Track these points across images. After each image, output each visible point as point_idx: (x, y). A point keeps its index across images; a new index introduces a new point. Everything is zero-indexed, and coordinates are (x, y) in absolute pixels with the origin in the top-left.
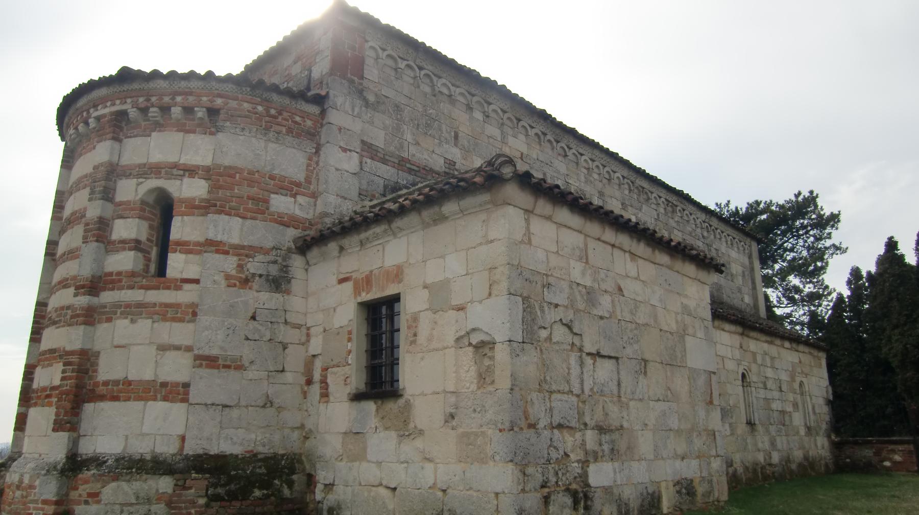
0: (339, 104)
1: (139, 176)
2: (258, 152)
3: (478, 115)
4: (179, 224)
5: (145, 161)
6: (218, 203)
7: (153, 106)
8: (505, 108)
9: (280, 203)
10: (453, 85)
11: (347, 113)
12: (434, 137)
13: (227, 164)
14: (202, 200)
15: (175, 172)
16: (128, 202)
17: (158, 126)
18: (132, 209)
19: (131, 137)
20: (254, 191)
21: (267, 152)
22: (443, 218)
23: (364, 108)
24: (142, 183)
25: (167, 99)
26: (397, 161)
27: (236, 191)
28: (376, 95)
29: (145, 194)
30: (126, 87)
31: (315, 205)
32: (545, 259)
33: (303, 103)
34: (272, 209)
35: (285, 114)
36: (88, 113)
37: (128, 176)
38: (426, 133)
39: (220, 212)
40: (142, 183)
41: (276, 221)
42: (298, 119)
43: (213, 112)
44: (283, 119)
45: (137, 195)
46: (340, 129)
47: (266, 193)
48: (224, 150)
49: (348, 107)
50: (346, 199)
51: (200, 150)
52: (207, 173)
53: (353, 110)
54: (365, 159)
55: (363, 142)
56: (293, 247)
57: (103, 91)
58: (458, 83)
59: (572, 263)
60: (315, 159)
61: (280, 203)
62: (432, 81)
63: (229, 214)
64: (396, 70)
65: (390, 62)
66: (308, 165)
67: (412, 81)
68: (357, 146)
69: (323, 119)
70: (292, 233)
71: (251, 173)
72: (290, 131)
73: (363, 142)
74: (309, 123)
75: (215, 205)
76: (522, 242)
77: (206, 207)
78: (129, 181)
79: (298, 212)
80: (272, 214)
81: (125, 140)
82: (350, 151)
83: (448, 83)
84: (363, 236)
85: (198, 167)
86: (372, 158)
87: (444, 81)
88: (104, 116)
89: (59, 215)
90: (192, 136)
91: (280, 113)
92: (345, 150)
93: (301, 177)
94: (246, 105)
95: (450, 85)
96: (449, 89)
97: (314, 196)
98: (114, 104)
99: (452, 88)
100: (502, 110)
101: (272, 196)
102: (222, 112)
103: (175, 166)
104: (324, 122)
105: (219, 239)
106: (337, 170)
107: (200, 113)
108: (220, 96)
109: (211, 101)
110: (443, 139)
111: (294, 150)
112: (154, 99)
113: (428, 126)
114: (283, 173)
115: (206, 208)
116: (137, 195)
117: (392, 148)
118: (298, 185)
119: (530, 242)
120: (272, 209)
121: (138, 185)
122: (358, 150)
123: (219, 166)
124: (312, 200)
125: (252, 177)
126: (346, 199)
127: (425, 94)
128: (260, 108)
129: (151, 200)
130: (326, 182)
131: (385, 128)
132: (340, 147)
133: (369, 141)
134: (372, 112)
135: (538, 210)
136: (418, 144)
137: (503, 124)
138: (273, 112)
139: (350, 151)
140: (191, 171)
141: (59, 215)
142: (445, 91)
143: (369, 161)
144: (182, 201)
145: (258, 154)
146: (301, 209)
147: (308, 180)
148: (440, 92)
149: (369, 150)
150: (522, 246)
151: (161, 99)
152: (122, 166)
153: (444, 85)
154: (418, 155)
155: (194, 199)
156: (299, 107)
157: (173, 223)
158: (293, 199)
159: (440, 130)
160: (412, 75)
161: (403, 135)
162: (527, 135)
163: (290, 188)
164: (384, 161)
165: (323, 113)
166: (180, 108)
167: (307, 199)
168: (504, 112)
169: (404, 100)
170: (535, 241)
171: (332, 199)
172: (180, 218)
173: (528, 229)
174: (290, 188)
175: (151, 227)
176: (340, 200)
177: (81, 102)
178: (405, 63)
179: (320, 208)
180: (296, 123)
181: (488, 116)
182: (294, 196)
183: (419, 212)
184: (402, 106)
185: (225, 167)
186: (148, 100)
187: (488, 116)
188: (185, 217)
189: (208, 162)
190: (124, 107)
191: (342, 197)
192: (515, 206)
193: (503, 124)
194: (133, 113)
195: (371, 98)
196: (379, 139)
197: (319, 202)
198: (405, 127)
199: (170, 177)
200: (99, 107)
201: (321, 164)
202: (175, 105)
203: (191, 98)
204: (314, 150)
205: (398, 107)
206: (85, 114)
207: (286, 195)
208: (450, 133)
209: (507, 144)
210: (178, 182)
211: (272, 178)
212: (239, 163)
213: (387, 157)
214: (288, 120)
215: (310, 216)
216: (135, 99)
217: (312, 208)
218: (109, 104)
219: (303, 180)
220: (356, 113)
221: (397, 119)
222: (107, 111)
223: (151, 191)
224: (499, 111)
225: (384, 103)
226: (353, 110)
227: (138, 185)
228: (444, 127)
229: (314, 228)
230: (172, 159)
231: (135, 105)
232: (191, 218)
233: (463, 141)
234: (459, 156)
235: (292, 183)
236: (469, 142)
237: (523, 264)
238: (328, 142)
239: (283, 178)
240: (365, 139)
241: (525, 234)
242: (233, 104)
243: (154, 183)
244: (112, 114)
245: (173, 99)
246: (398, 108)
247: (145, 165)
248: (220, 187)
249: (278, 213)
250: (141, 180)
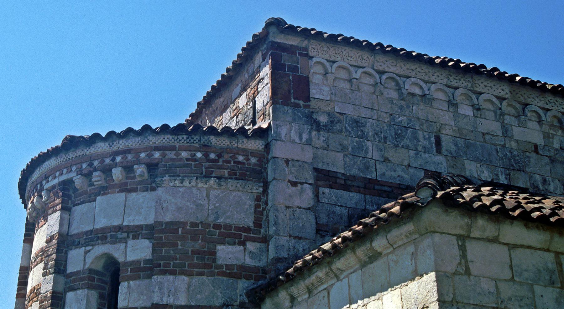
0: (283, 135)
1: (86, 244)
2: (200, 202)
3: (466, 110)
4: (125, 291)
5: (90, 228)
6: (162, 263)
7: (95, 170)
8: (502, 94)
9: (227, 254)
10: (426, 82)
11: (293, 142)
12: (408, 148)
13: (168, 220)
14: (146, 261)
15: (120, 235)
16: (78, 273)
17: (103, 190)
18: (82, 279)
19: (78, 204)
20: (198, 245)
21: (209, 200)
22: (375, 256)
23: (314, 133)
24: (89, 251)
25: (108, 161)
26: (362, 184)
27: (180, 247)
28: (329, 114)
29: (92, 263)
30: (71, 155)
31: (268, 251)
32: (493, 289)
33: (245, 140)
34: (220, 262)
35: (226, 156)
36: (41, 185)
37: (78, 245)
38: (397, 146)
39: (163, 273)
40: (89, 251)
41: (223, 274)
42: (241, 158)
43: (152, 167)
44: (224, 162)
45: (85, 264)
46: (287, 161)
47: (211, 246)
48: (164, 205)
49: (294, 135)
50: (300, 238)
51: (141, 208)
52: (148, 231)
53: (301, 138)
54: (321, 190)
55: (316, 170)
56: (247, 301)
57: (52, 163)
58: (432, 79)
59: (538, 289)
60: (264, 199)
61: (227, 254)
62: (397, 84)
63: (173, 273)
64: (350, 81)
65: (343, 74)
66: (257, 206)
67: (372, 90)
68: (309, 176)
69: (268, 154)
70: (243, 285)
71: (194, 225)
72: (233, 175)
73: (316, 170)
74: (253, 160)
75: (159, 265)
76: (456, 273)
77: (146, 270)
78: (77, 250)
79: (249, 262)
80: (221, 266)
81: (73, 209)
82: (302, 183)
83: (419, 81)
84: (308, 281)
85: (141, 227)
86: (330, 187)
87: (413, 80)
88: (54, 187)
89: (23, 292)
90: (134, 195)
91: (219, 156)
92: (294, 184)
93: (249, 222)
94: (184, 154)
95: (421, 83)
96: (421, 87)
97: (265, 240)
98: (61, 174)
99: (424, 86)
100: (498, 97)
101: (219, 247)
102: (160, 165)
103: (119, 228)
104: (269, 158)
105: (165, 302)
106: (287, 207)
107: (140, 170)
108: (157, 149)
109: (149, 156)
110: (420, 148)
111: (239, 193)
112: (96, 163)
113: (398, 136)
114: (228, 221)
115: (151, 269)
116: (85, 264)
117: (354, 172)
118: (247, 230)
119: (468, 272)
120: (220, 262)
121: (86, 252)
122: (311, 181)
123: (160, 223)
124: (263, 246)
125: (196, 230)
126: (300, 238)
127: (391, 101)
128: (199, 155)
129: (99, 266)
130: (276, 223)
131: (344, 148)
132: (289, 181)
133: (325, 167)
134: (326, 135)
135: (475, 233)
136: (386, 160)
137: (502, 114)
138: (212, 156)
139: (302, 183)
140: (135, 232)
141: (23, 292)
142: (417, 91)
143: (327, 190)
144: (126, 264)
145: (201, 205)
146: (251, 258)
147: (258, 224)
148: (409, 93)
149: (325, 177)
150: (457, 278)
151: (102, 161)
152: (72, 236)
153: (415, 84)
154: (388, 174)
155: (138, 262)
156: (240, 146)
157: (120, 291)
158: (242, 248)
159: (416, 138)
160: (372, 82)
161: (366, 153)
162: (540, 122)
163: (237, 235)
164: (346, 187)
165: (267, 147)
166: (120, 169)
167: (258, 245)
168: (501, 99)
169: (365, 113)
170: (474, 269)
171: (284, 240)
172: (126, 283)
173: (464, 256)
174: (237, 235)
175: (101, 296)
176: (293, 241)
177: (36, 176)
178: (361, 70)
179: (272, 254)
180: (239, 163)
181: (479, 109)
182: (243, 244)
183: (353, 250)
184: (363, 121)
185: (167, 223)
186: (91, 165)
187: (479, 109)
188: (131, 282)
189: (150, 220)
190: (70, 175)
191: (295, 238)
192: (442, 233)
193: (502, 114)
194: (78, 181)
195: (323, 119)
196: (337, 163)
197: (271, 247)
198: (369, 144)
199: (115, 241)
200: (50, 179)
201: (270, 204)
202: (116, 165)
203: (130, 157)
204: (261, 189)
205: (357, 122)
206: (39, 186)
207: (234, 244)
208: (429, 138)
209: (512, 137)
210: (122, 246)
211: (217, 227)
212: (182, 218)
213: (349, 182)
214: (229, 162)
215: (262, 264)
216: (79, 166)
217: (265, 254)
218: (57, 174)
219: (251, 225)
220: (304, 140)
221: (358, 137)
222: (56, 181)
223: (98, 258)
224: (495, 100)
225: (339, 121)
226: (301, 138)
227: (86, 252)
228: (420, 134)
229: (268, 276)
230: (116, 222)
231: (80, 172)
232: (137, 282)
233: (447, 143)
234: (445, 164)
235: (238, 229)
236: (456, 145)
237: (459, 299)
238: (274, 179)
239: (228, 227)
240: (320, 166)
241: (460, 264)
242: (171, 155)
243: (100, 249)
244: (60, 183)
245: (113, 160)
246: (357, 123)
247: (91, 231)
248: (164, 245)
249: (227, 266)
250: (88, 248)
